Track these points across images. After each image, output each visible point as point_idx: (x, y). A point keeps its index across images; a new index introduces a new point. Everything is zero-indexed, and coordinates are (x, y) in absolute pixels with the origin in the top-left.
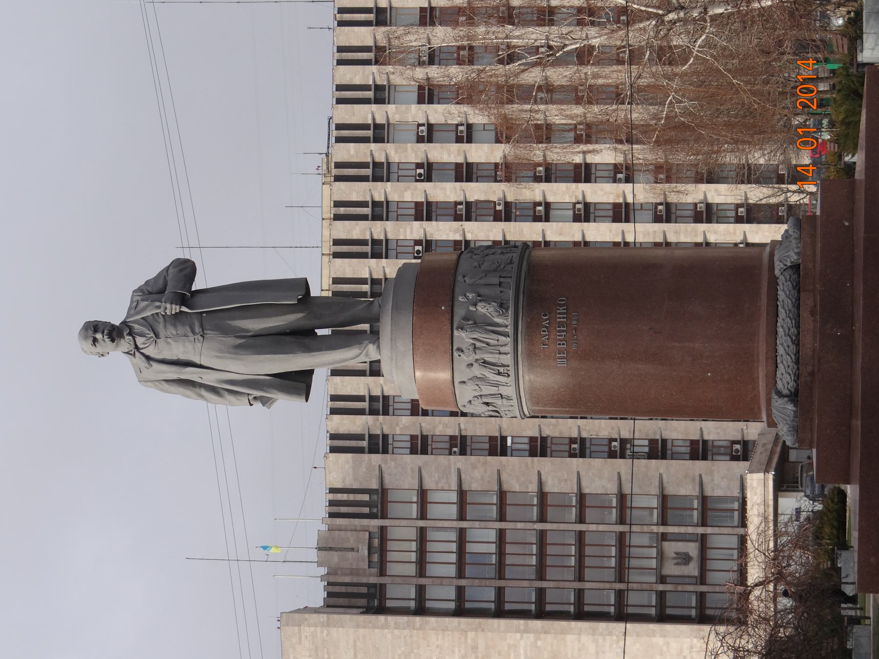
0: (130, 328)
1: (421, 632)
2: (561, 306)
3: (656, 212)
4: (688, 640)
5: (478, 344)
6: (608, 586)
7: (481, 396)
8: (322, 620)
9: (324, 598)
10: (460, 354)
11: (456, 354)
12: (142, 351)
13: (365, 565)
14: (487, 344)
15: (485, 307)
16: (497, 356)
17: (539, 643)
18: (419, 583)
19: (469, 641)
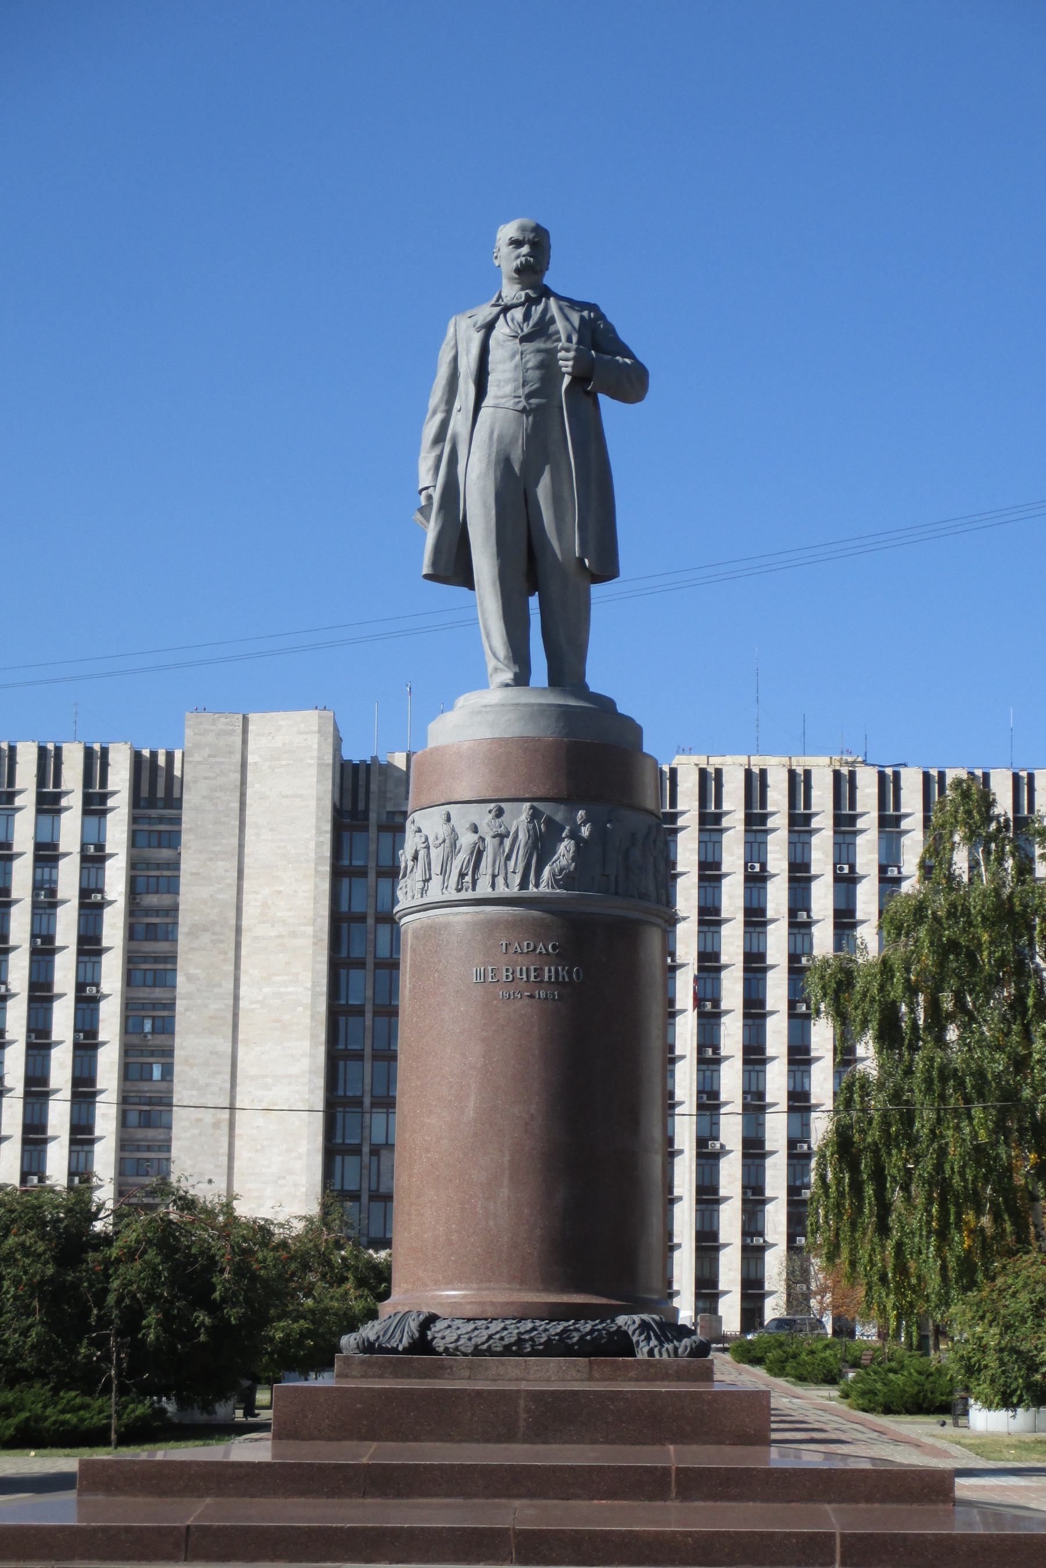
0: (537, 301)
1: (313, 872)
2: (569, 973)
3: (801, 1142)
4: (304, 1182)
5: (507, 842)
6: (367, 1088)
7: (428, 848)
8: (326, 757)
9: (351, 761)
10: (493, 812)
11: (492, 806)
12: (502, 316)
13: (390, 808)
14: (508, 854)
15: (568, 852)
16: (490, 871)
17: (301, 1009)
18: (369, 870)
19: (302, 928)
